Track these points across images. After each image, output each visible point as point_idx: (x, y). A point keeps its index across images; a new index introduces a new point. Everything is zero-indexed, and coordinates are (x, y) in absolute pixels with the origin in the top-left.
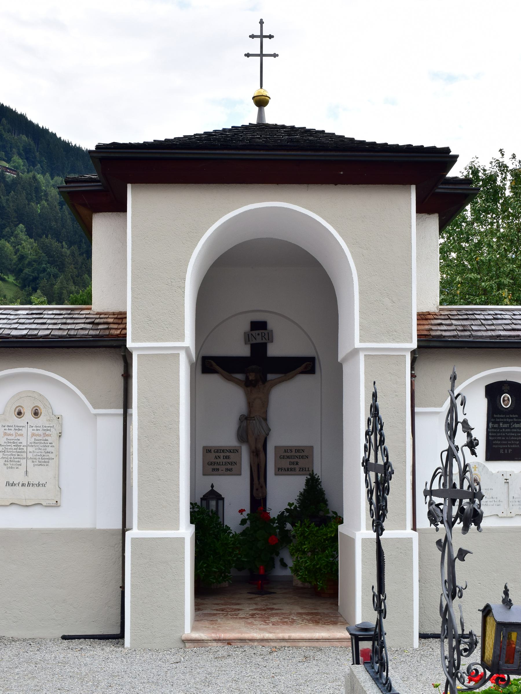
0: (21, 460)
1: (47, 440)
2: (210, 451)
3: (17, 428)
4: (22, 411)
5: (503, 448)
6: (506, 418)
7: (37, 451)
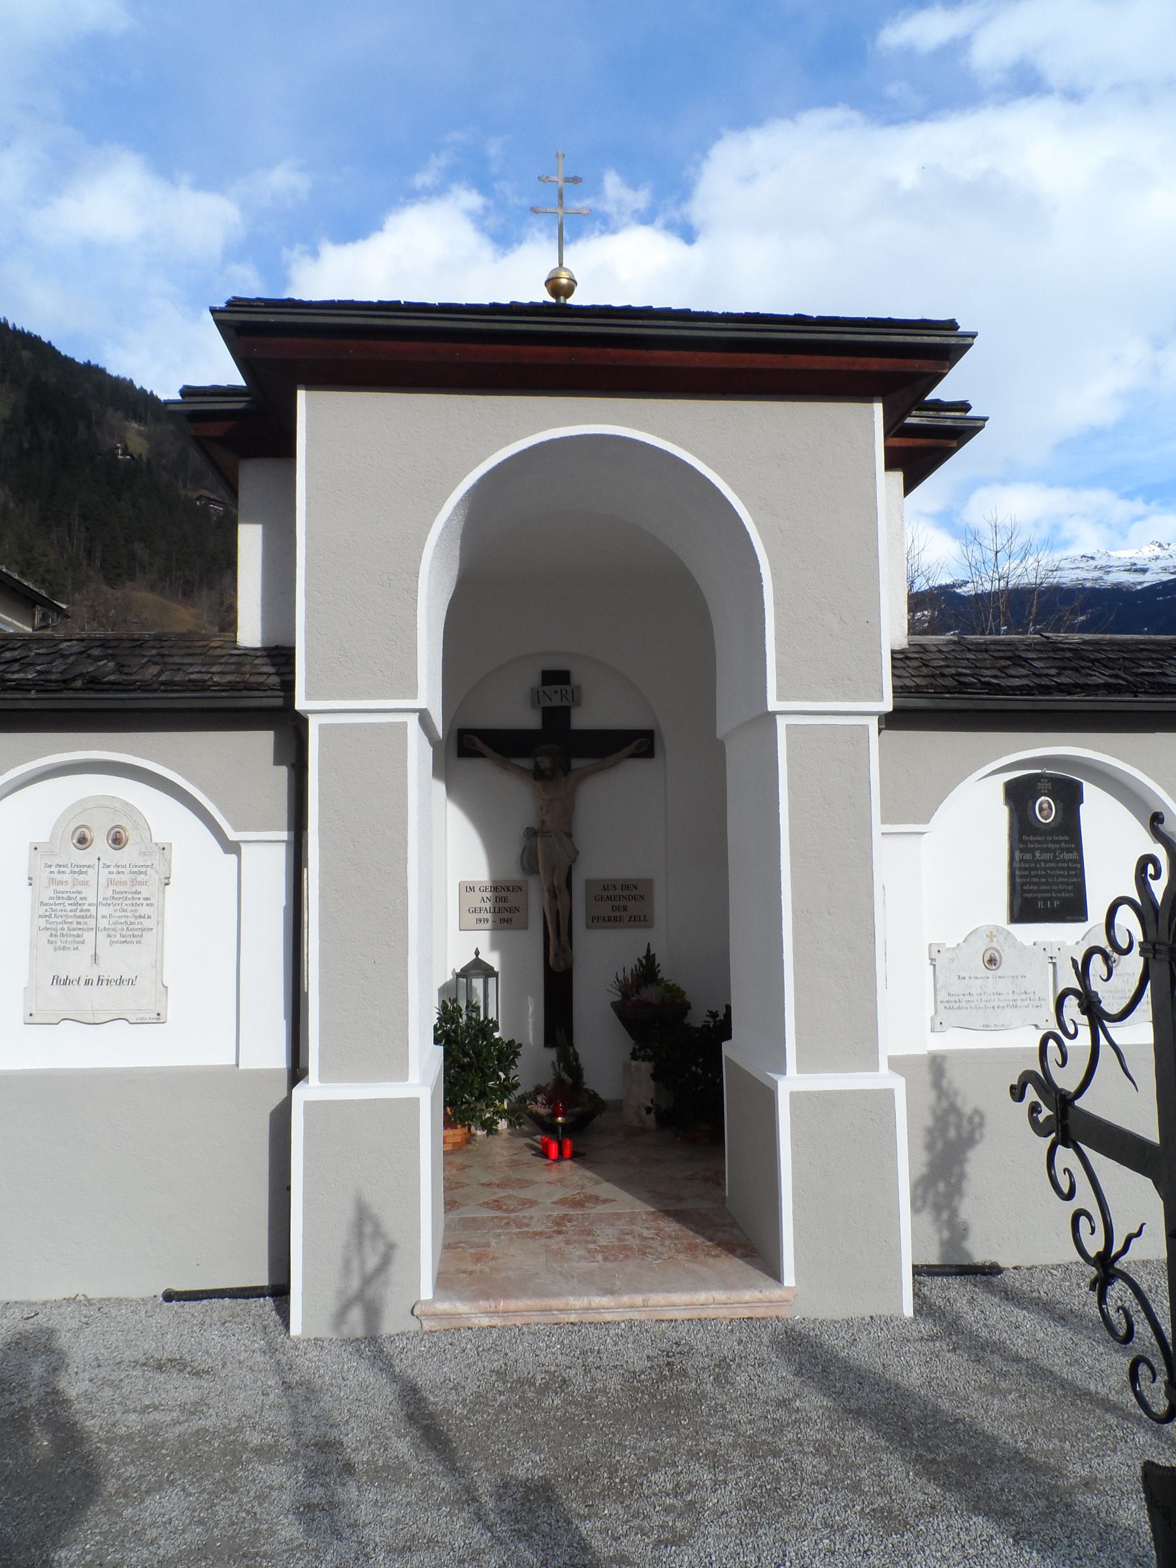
0: (85, 933)
1: (139, 893)
2: (472, 889)
3: (76, 869)
4: (88, 836)
5: (1042, 899)
6: (1046, 842)
7: (118, 914)
